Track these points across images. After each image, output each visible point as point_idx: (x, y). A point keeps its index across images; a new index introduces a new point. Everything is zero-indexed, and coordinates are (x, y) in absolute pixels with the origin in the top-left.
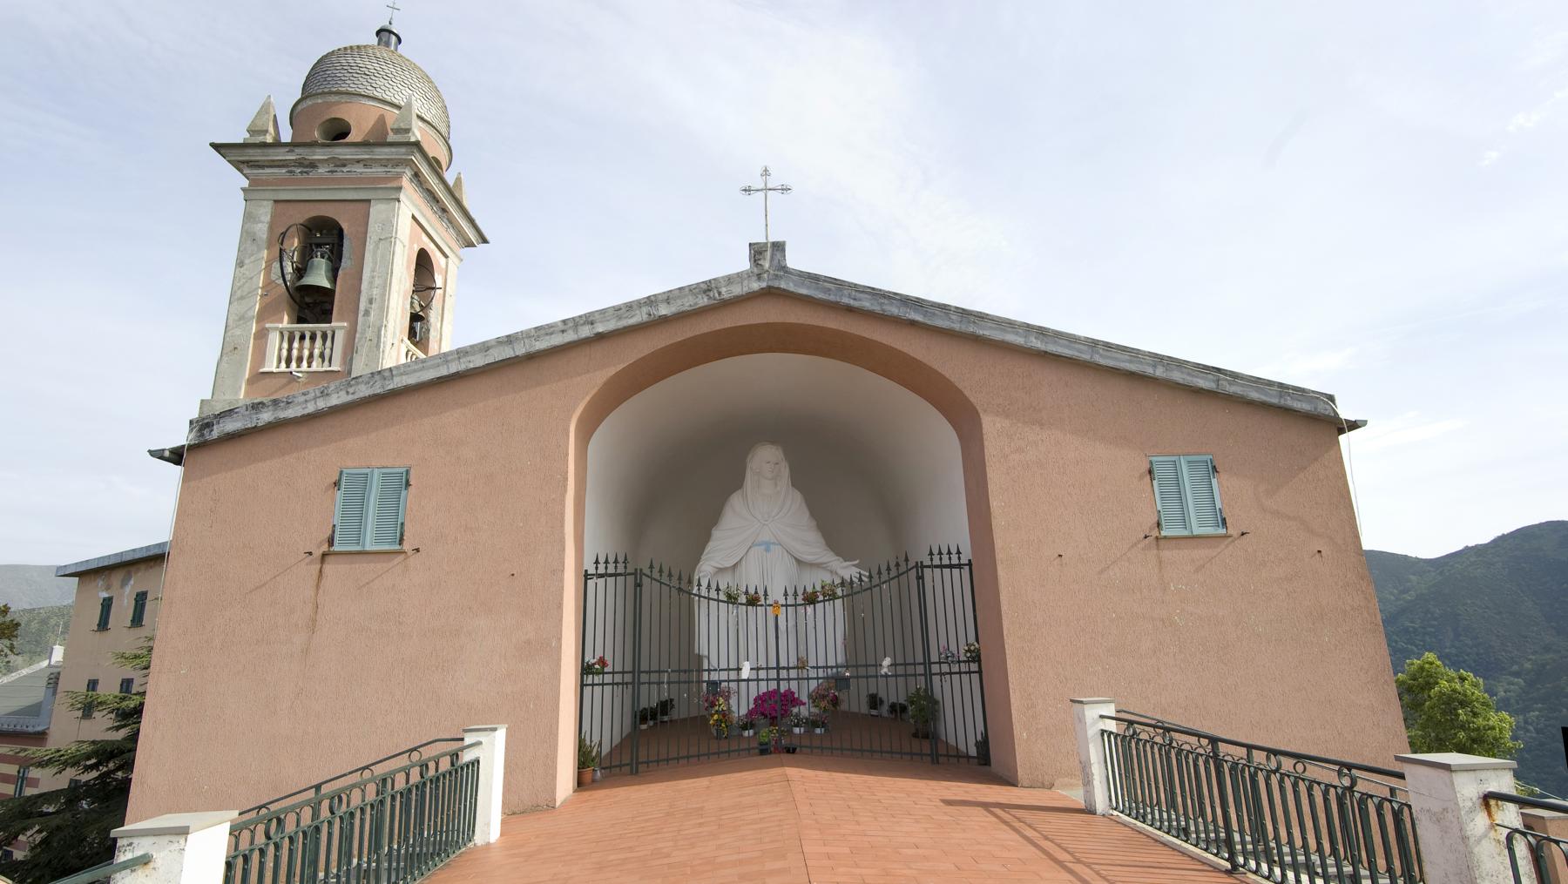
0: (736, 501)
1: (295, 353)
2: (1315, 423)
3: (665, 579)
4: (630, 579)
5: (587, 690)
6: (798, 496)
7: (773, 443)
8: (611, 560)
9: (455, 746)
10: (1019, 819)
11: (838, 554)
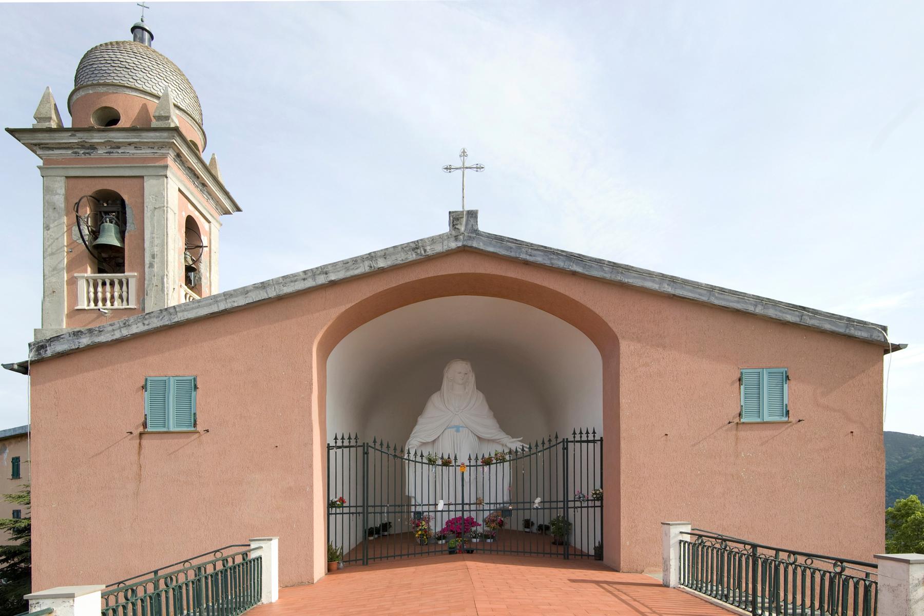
0: (435, 398)
1: (100, 295)
4: (360, 450)
5: (332, 517)
7: (463, 359)
8: (346, 437)
9: (244, 549)
10: (619, 590)
11: (507, 433)
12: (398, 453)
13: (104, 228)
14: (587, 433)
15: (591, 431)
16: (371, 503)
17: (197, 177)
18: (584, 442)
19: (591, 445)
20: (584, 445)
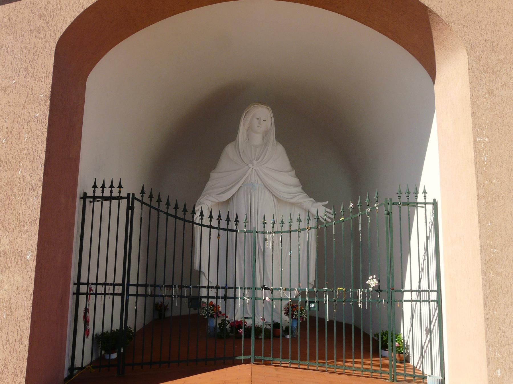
0: (229, 150)
3: (154, 204)
4: (124, 203)
5: (434, 286)
6: (280, 149)
8: (108, 185)
12: (188, 217)
14: (112, 186)
15: (116, 184)
16: (259, 285)
18: (115, 198)
19: (115, 203)
20: (106, 203)
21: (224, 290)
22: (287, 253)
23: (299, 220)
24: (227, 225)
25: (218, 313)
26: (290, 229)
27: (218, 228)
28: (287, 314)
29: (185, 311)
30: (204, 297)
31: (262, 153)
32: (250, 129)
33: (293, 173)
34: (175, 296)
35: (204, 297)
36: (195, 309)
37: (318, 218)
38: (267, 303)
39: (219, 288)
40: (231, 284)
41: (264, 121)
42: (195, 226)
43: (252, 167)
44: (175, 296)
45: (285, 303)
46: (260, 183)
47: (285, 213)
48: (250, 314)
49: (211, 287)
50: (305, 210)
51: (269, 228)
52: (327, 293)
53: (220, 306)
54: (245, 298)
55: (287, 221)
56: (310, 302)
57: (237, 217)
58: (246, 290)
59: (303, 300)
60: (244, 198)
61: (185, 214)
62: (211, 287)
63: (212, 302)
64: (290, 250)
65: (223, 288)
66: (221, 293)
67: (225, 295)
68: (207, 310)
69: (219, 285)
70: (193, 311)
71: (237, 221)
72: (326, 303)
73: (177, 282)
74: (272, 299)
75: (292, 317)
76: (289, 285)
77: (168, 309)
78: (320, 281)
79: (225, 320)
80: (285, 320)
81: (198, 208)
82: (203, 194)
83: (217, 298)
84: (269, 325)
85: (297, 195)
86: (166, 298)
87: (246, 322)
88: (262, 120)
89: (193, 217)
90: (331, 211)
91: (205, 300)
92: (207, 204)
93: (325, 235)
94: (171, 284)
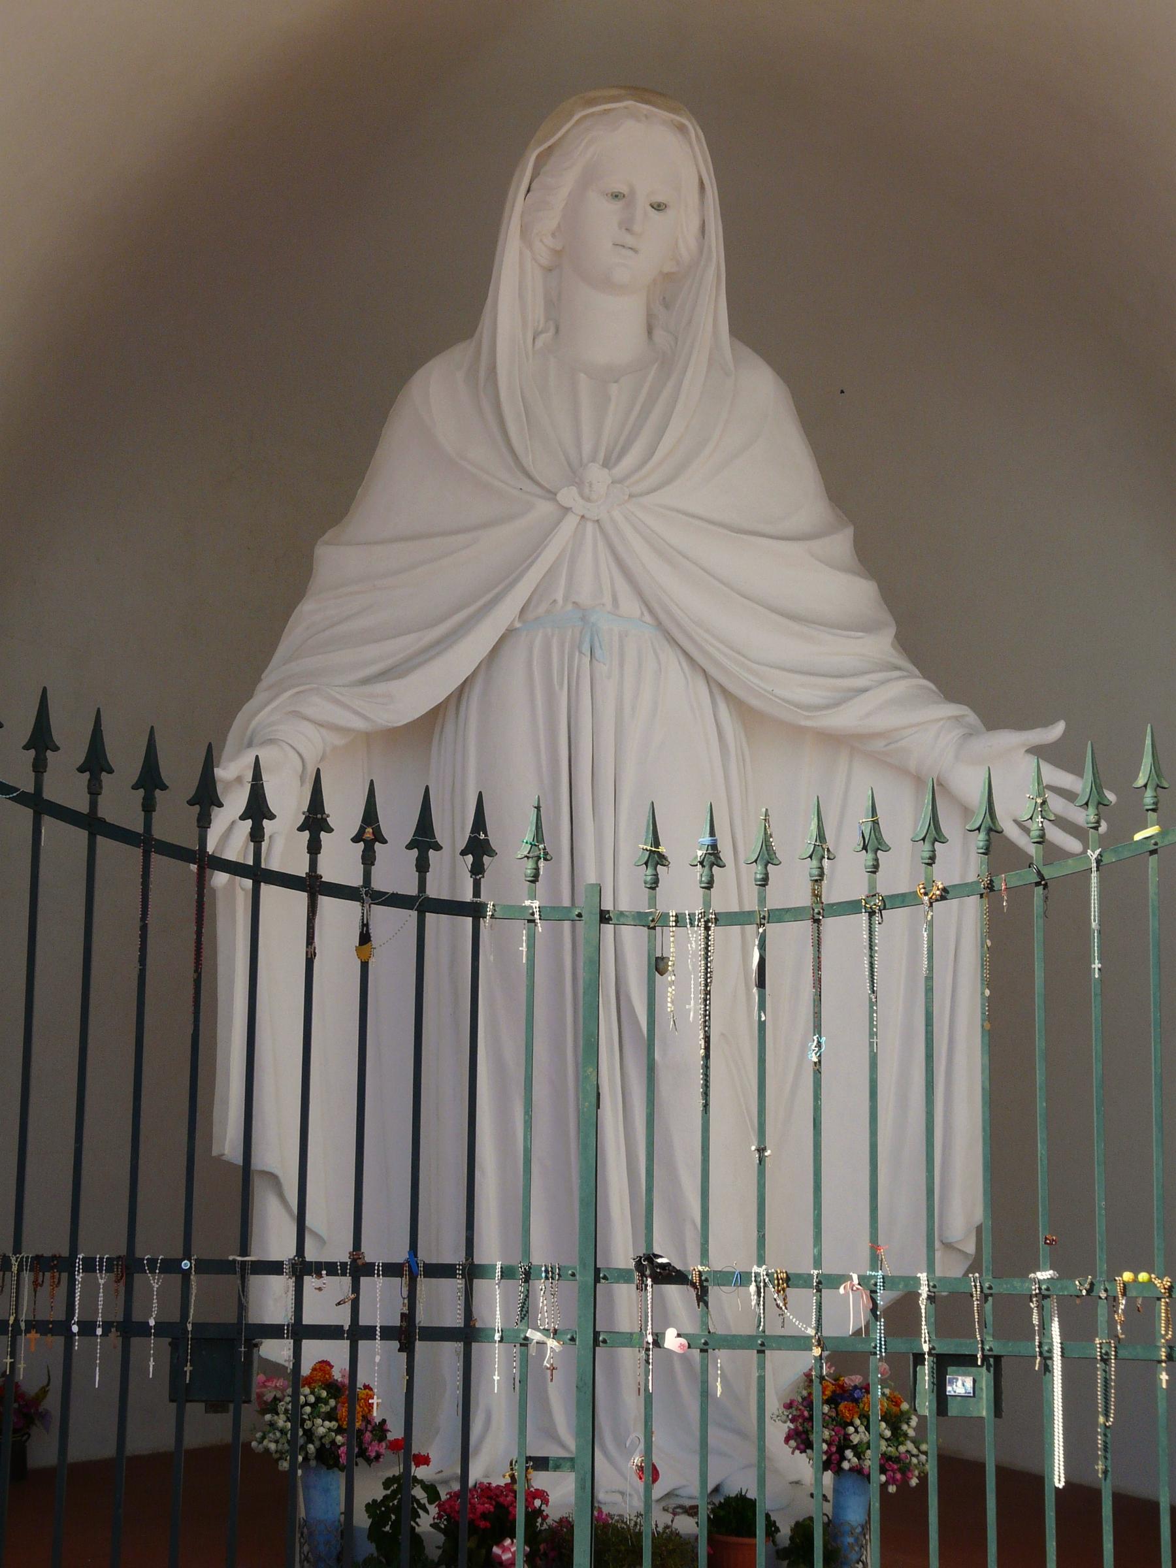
0: (435, 395)
2: (332, 1367)
6: (761, 388)
10: (595, 546)
11: (951, 689)
12: (172, 822)
13: (213, 891)
16: (622, 1252)
17: (722, 642)
21: (398, 1285)
22: (804, 1050)
23: (874, 843)
24: (427, 873)
25: (363, 1440)
26: (817, 896)
27: (364, 894)
28: (801, 1439)
29: (151, 1434)
30: (275, 1331)
31: (645, 412)
32: (566, 263)
33: (841, 543)
34: (87, 1328)
35: (275, 1331)
36: (216, 1406)
37: (993, 830)
38: (678, 1366)
39: (368, 1270)
40: (443, 1247)
41: (658, 207)
42: (220, 879)
43: (579, 506)
44: (87, 1328)
45: (788, 1370)
46: (630, 606)
47: (790, 797)
48: (565, 1437)
49: (317, 1269)
50: (918, 780)
51: (681, 890)
52: (1052, 1305)
53: (375, 1385)
54: (535, 1336)
55: (793, 844)
56: (945, 1363)
57: (480, 822)
58: (540, 1285)
59: (900, 1345)
60: (532, 701)
61: (148, 807)
62: (317, 1269)
63: (324, 1366)
64: (818, 1029)
65: (391, 1270)
66: (381, 1301)
67: (409, 1317)
68: (295, 1417)
69: (372, 1253)
70: (206, 1428)
71: (478, 848)
72: (1047, 1369)
73: (103, 1238)
74: (705, 1344)
75: (832, 1463)
76: (810, 1251)
77: (44, 1416)
78: (1008, 1237)
79: (401, 1484)
80: (792, 1481)
81: (232, 772)
82: (270, 676)
83: (357, 1333)
84: (692, 1511)
85: (861, 682)
86: (29, 1341)
87: (542, 1495)
88: (642, 203)
89: (204, 822)
90: (1079, 785)
91: (277, 1351)
92: (295, 741)
93: (1038, 936)
94: (62, 1317)
